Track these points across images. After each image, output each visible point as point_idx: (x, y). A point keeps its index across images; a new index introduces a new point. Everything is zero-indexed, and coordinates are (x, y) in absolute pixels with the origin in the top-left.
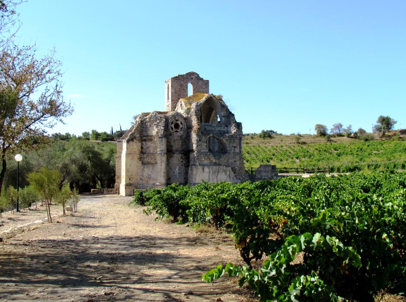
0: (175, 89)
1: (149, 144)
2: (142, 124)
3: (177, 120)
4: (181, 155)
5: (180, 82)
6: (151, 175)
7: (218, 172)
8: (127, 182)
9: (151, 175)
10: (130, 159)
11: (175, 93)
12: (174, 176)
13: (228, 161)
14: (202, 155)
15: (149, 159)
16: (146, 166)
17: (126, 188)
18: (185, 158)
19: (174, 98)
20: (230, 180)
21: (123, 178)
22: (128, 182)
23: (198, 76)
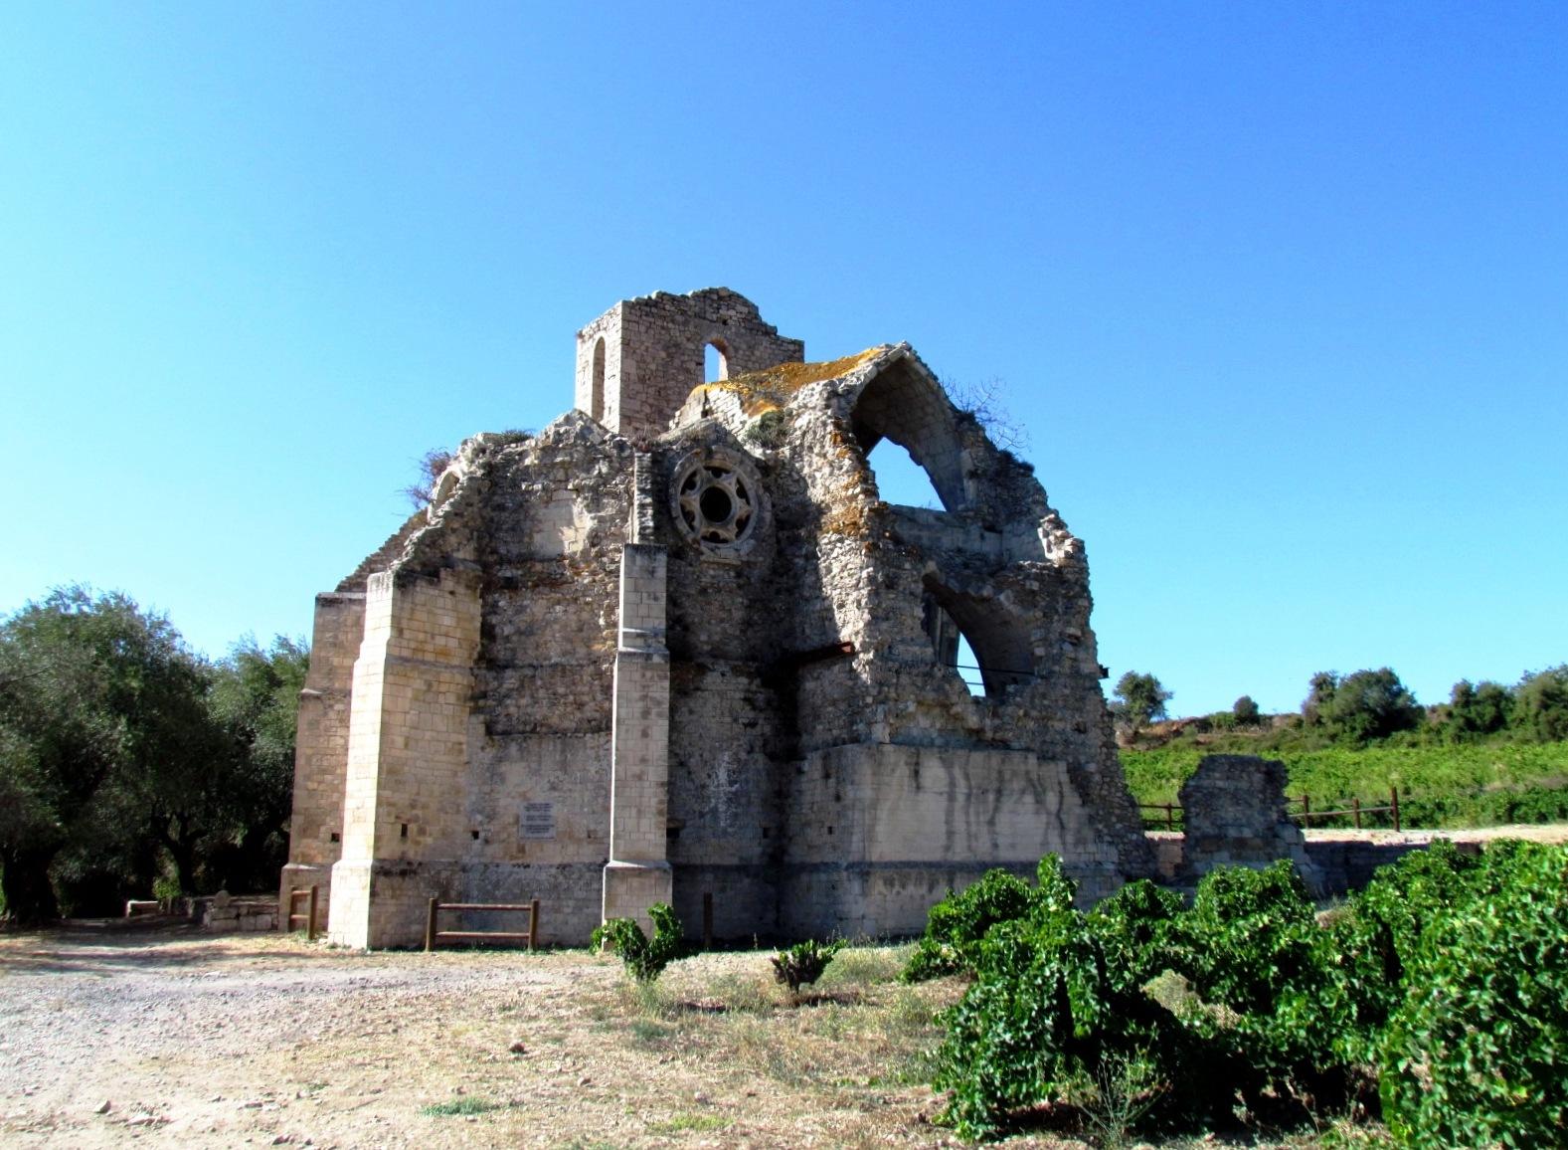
0: (641, 362)
1: (537, 606)
2: (494, 484)
3: (718, 472)
4: (744, 680)
5: (668, 329)
6: (547, 806)
7: (999, 792)
8: (384, 854)
9: (547, 806)
10: (409, 694)
11: (642, 380)
12: (702, 815)
13: (1044, 721)
14: (905, 679)
15: (536, 701)
16: (513, 749)
17: (373, 894)
18: (769, 702)
19: (637, 405)
20: (1064, 843)
21: (357, 820)
22: (394, 849)
23: (752, 312)
